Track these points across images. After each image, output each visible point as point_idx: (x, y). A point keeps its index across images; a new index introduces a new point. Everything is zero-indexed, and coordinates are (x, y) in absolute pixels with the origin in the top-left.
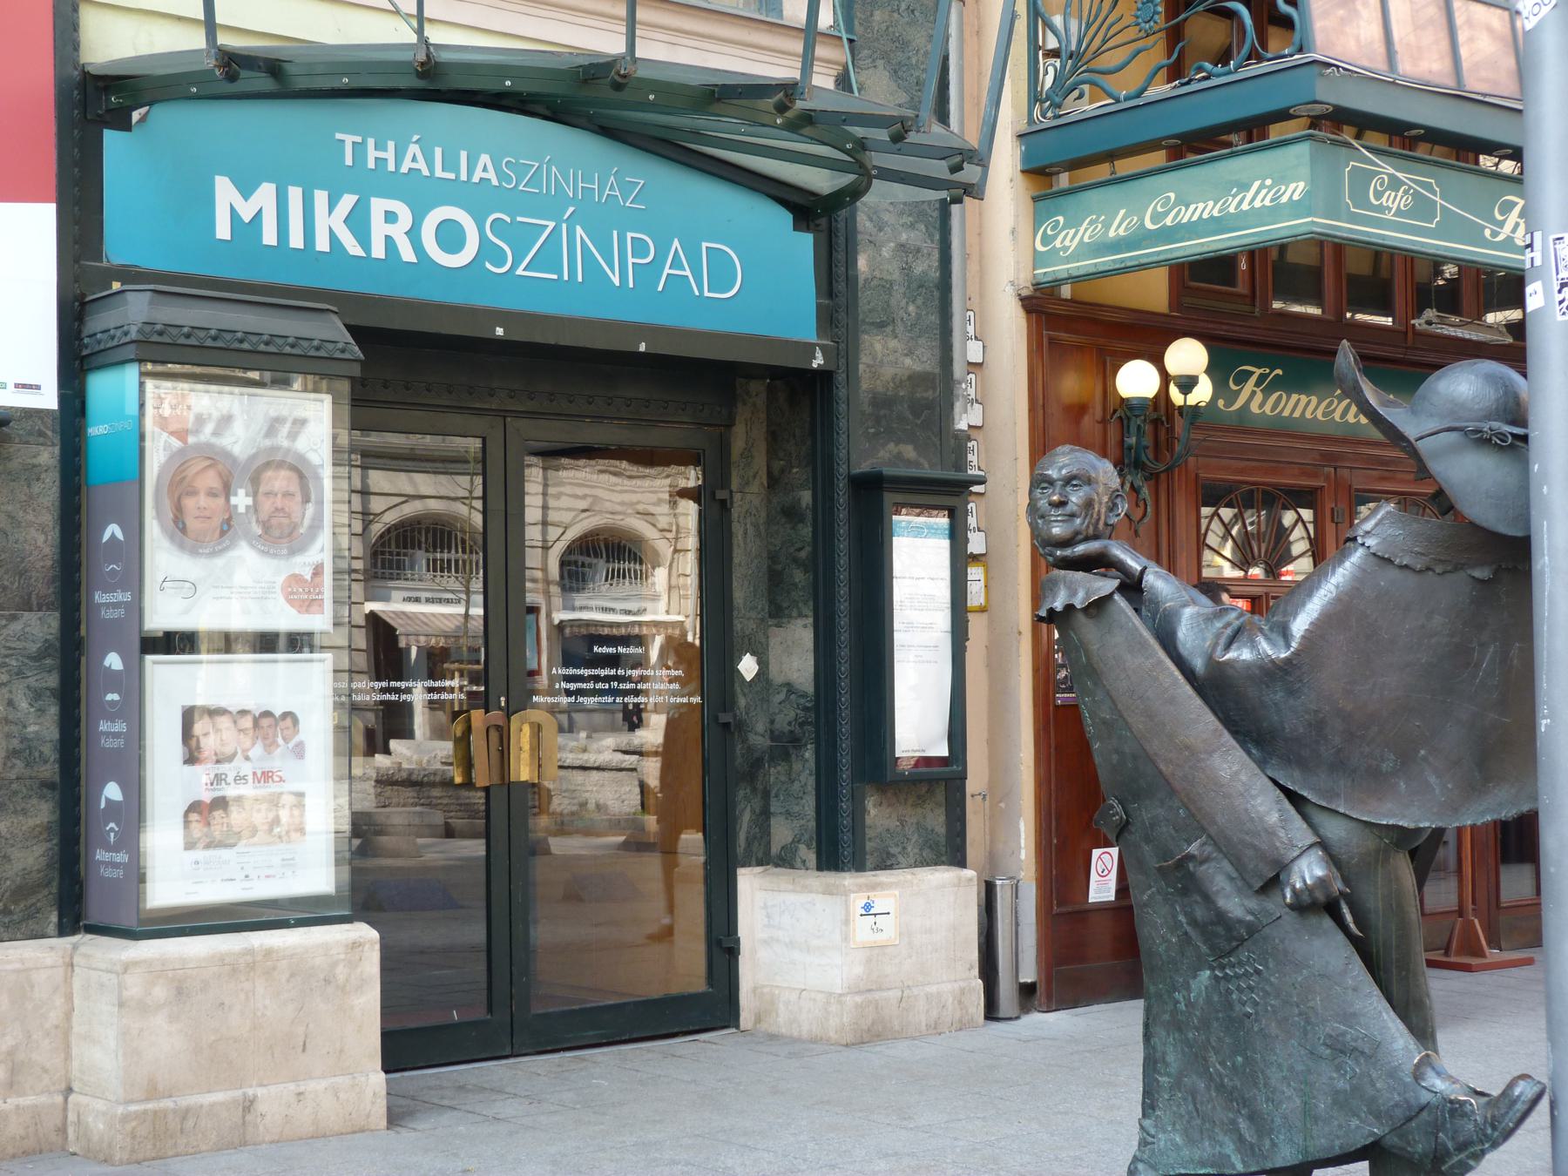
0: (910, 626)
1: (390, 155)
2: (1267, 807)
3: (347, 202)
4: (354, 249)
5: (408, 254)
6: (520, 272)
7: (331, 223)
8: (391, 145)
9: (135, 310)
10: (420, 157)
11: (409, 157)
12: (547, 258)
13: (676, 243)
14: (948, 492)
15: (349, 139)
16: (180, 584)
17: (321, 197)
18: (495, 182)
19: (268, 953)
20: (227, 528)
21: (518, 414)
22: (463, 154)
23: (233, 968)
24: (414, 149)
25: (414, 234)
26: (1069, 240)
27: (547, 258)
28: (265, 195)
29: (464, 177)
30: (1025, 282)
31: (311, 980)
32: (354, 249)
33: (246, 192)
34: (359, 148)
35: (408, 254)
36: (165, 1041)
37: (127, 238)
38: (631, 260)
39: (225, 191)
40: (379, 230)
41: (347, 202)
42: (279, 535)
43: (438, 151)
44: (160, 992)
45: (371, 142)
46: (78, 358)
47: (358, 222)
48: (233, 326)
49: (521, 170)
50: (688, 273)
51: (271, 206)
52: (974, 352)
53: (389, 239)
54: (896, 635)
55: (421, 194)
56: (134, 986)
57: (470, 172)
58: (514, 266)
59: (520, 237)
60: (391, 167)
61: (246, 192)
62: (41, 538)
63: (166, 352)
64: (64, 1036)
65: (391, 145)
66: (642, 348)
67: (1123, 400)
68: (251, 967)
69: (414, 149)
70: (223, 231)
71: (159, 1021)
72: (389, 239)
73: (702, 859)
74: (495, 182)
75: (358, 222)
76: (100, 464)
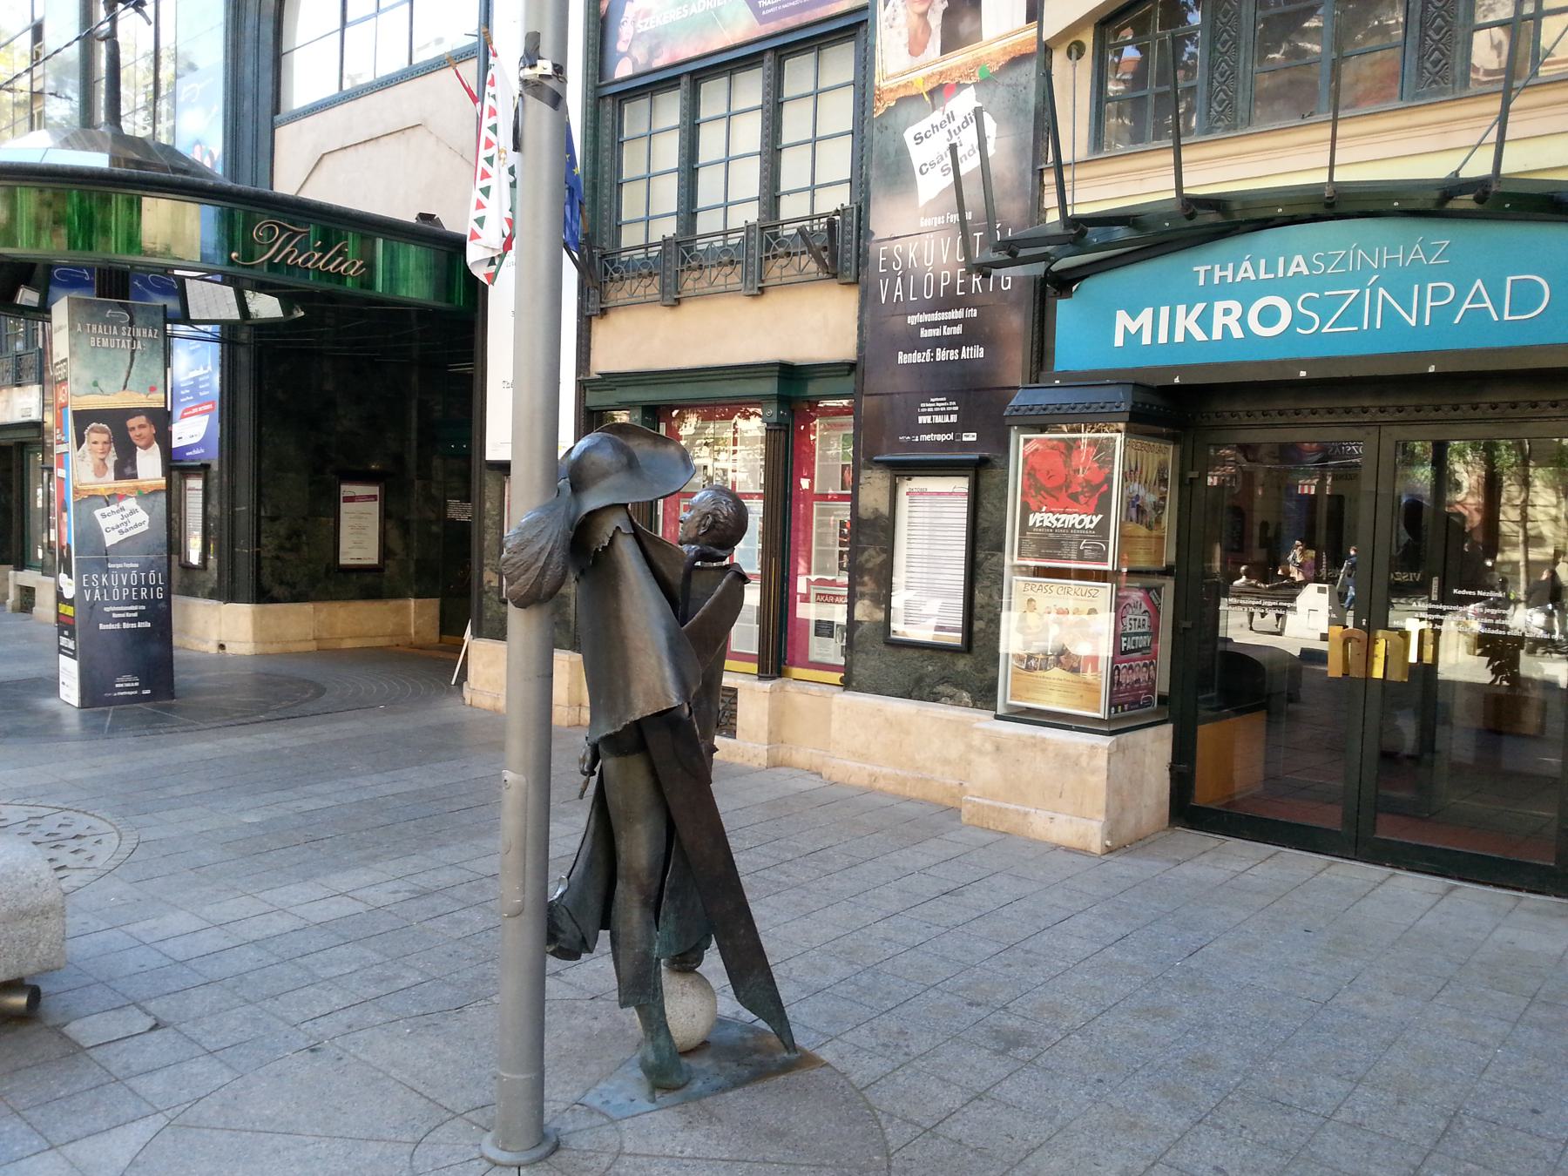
1: (1229, 273)
3: (1199, 307)
4: (1200, 336)
5: (1237, 333)
6: (1325, 330)
7: (1187, 322)
8: (1231, 265)
10: (1302, 263)
11: (1294, 264)
13: (1479, 283)
15: (1202, 269)
17: (1181, 309)
18: (1306, 272)
19: (1044, 740)
21: (1391, 423)
22: (1281, 260)
24: (1247, 264)
25: (1242, 321)
28: (1146, 315)
29: (1281, 274)
31: (1066, 760)
32: (1200, 336)
33: (1134, 316)
34: (1209, 274)
35: (1237, 333)
38: (1429, 304)
39: (1122, 318)
40: (1218, 321)
41: (1199, 307)
43: (1263, 262)
44: (989, 747)
45: (1217, 267)
47: (1205, 321)
49: (1327, 260)
50: (1488, 304)
53: (1225, 327)
54: (963, 554)
55: (1246, 293)
56: (977, 740)
57: (1285, 271)
58: (1322, 325)
59: (1325, 307)
60: (1230, 280)
61: (1134, 316)
65: (1231, 265)
66: (1432, 369)
68: (1035, 745)
69: (1247, 264)
70: (1119, 341)
71: (987, 760)
72: (1225, 327)
73: (412, 602)
74: (1306, 272)
75: (1205, 321)
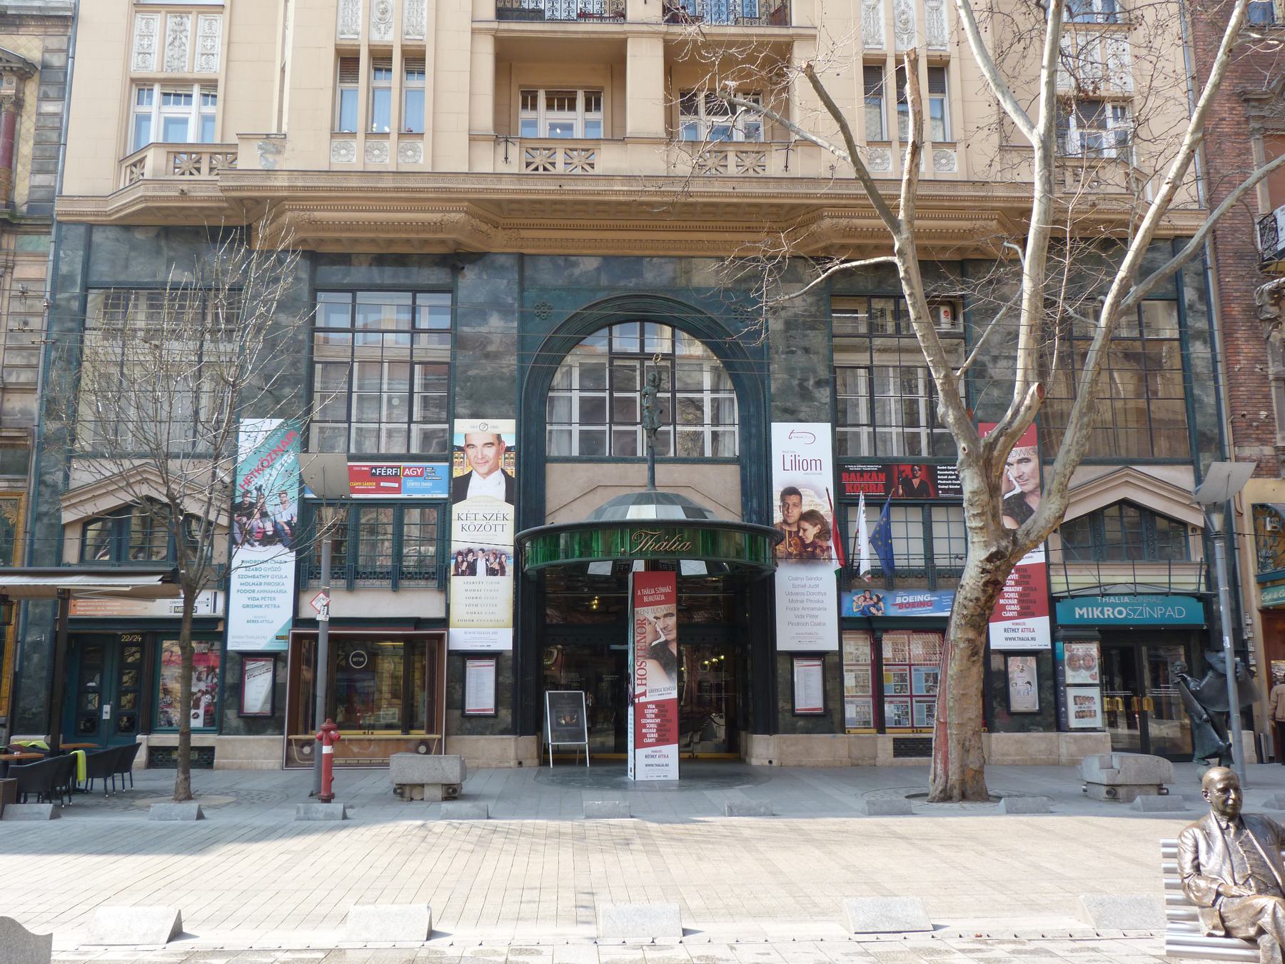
0: (498, 625)
2: (1199, 707)
7: (1097, 613)
9: (1062, 633)
12: (1141, 614)
14: (65, 595)
16: (1071, 676)
20: (1080, 667)
23: (1084, 738)
26: (1268, 597)
27: (1141, 614)
30: (1260, 606)
36: (1073, 748)
37: (1061, 620)
39: (1077, 610)
42: (1089, 668)
46: (1054, 640)
48: (1079, 632)
51: (1083, 613)
52: (1249, 621)
59: (1134, 611)
62: (649, 637)
63: (1070, 640)
64: (1058, 747)
67: (988, 622)
75: (1102, 612)
76: (1059, 656)
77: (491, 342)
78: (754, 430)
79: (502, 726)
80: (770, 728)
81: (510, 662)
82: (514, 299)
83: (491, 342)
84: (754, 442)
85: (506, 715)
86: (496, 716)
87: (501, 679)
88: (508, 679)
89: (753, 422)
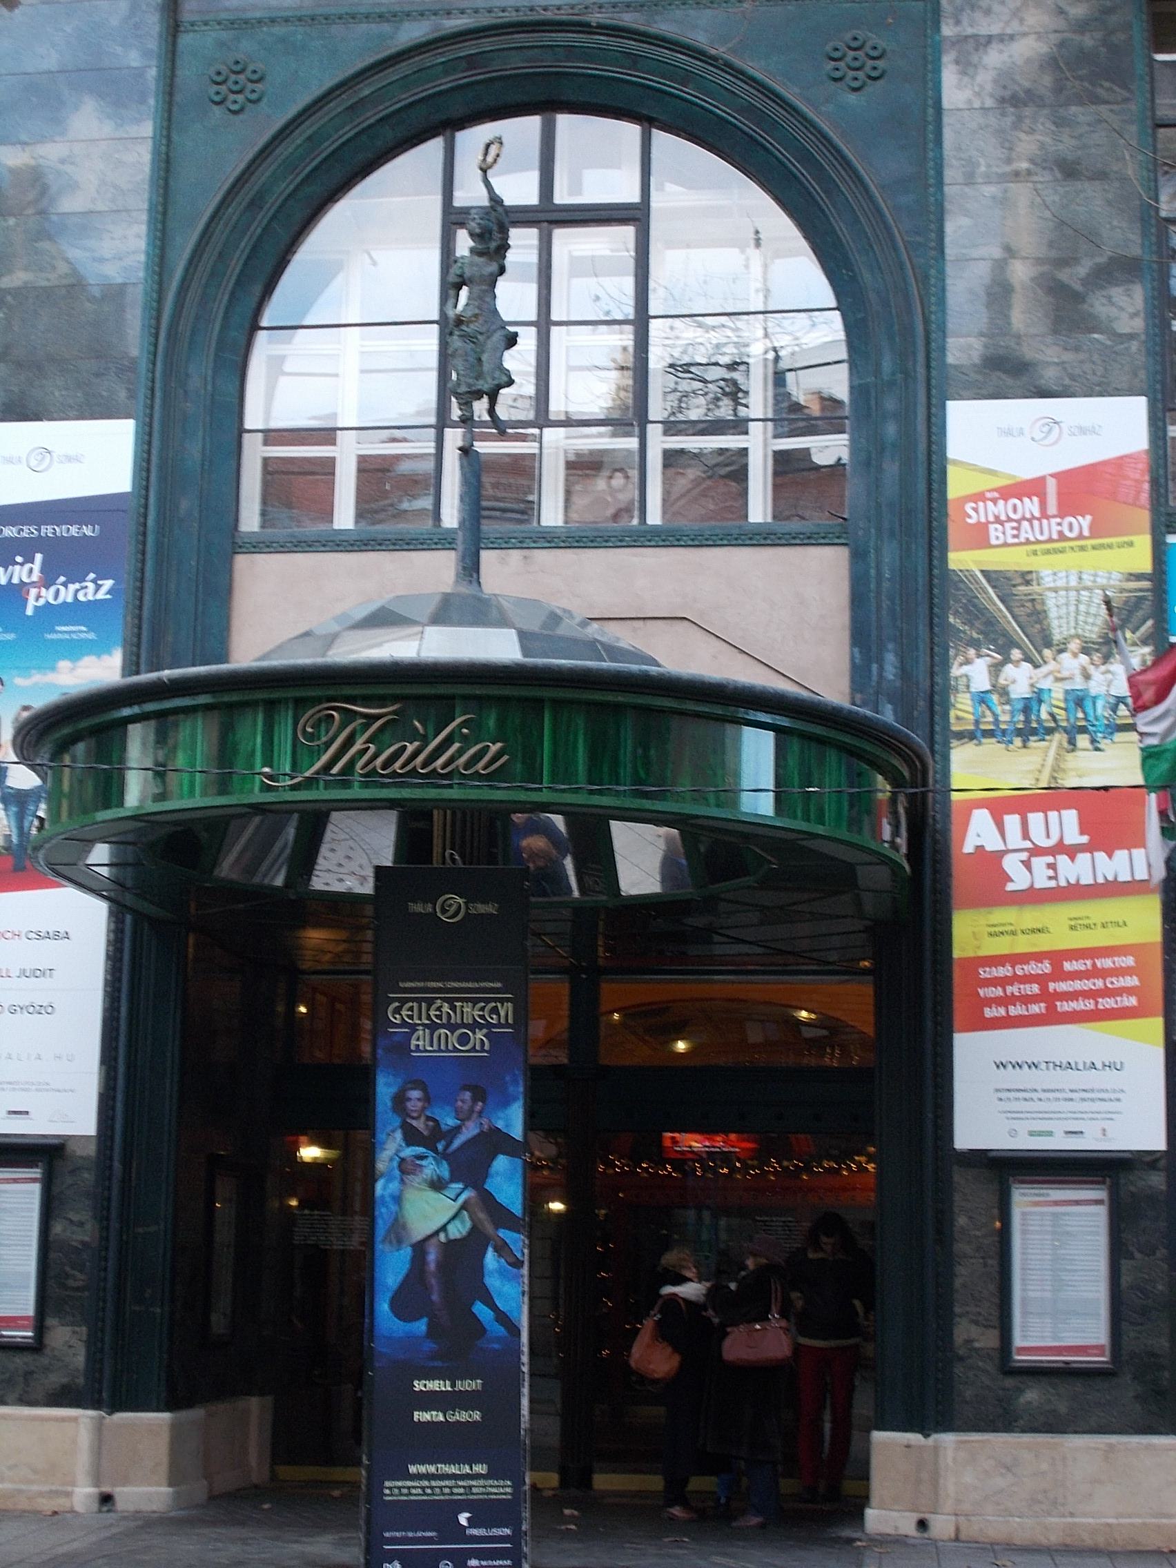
77: (73, 186)
78: (891, 430)
79: (56, 1379)
80: (929, 1411)
81: (88, 1177)
82: (146, 54)
83: (73, 186)
84: (891, 469)
85: (68, 1340)
86: (37, 1347)
87: (57, 1228)
88: (80, 1228)
89: (890, 404)
